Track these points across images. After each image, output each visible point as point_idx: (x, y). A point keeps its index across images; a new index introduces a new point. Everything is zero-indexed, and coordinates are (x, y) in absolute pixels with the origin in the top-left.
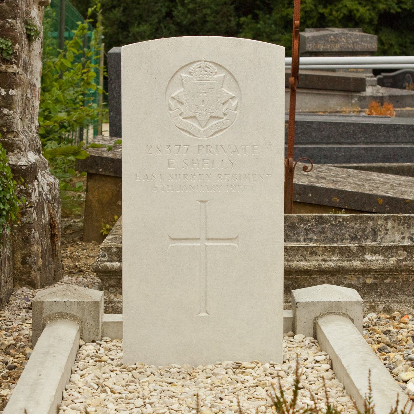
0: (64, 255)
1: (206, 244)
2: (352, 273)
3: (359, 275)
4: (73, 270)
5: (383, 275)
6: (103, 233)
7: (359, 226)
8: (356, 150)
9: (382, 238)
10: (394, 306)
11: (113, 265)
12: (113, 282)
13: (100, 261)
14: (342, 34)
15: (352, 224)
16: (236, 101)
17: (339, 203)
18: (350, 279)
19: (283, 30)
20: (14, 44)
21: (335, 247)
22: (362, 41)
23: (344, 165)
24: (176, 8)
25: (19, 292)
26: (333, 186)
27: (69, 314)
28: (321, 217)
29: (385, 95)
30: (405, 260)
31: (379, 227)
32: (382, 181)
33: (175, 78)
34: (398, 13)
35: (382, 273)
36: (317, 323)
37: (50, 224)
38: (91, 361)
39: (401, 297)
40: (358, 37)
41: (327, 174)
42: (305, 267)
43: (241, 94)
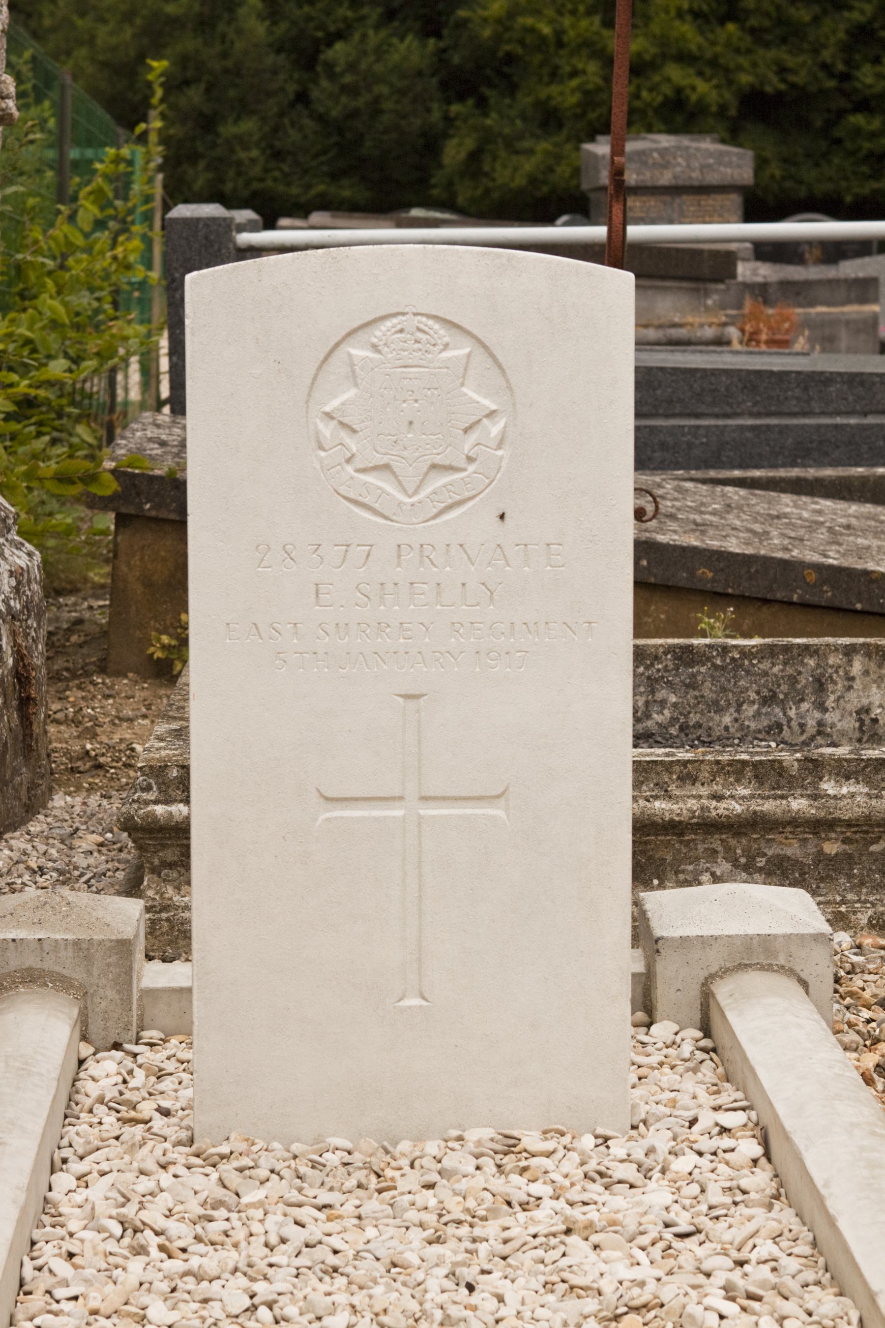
0: (59, 716)
1: (422, 812)
2: (788, 829)
3: (805, 832)
4: (79, 763)
5: (866, 832)
6: (153, 654)
7: (782, 671)
8: (733, 431)
9: (839, 698)
11: (171, 813)
12: (170, 855)
13: (137, 801)
14: (678, 148)
15: (765, 665)
16: (502, 424)
17: (713, 580)
18: (781, 843)
19: (539, 132)
21: (744, 763)
23: (712, 474)
26: (696, 539)
27: (51, 973)
28: (689, 649)
29: (769, 280)
31: (830, 671)
32: (806, 520)
33: (333, 360)
34: (779, 94)
36: (713, 995)
37: (17, 672)
38: (110, 1120)
40: (711, 154)
41: (677, 504)
42: (667, 814)
43: (514, 405)
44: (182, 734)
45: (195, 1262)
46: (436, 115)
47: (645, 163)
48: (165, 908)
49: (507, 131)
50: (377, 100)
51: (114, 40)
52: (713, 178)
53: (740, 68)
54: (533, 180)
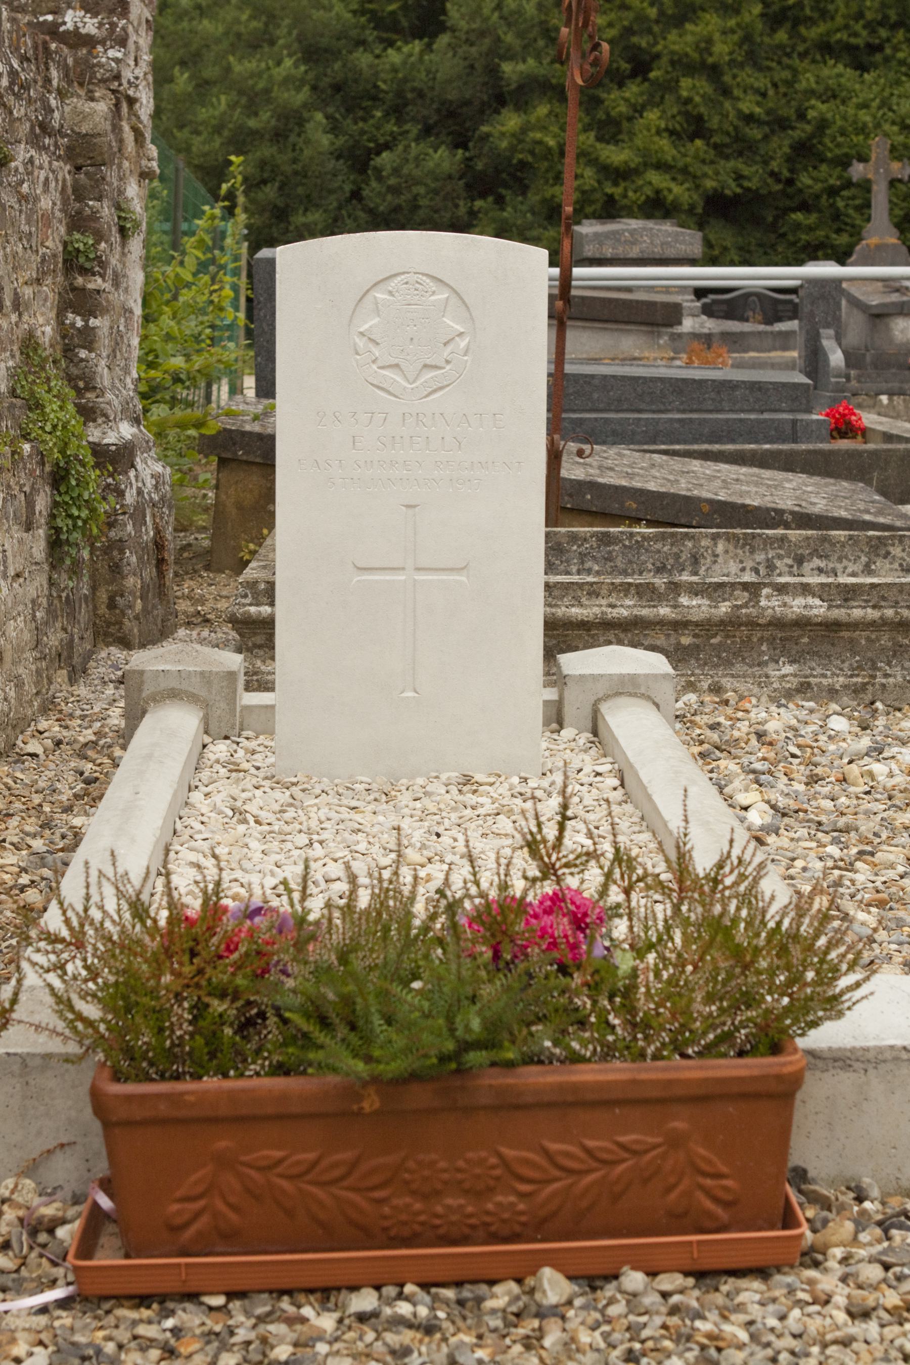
10: (726, 682)
12: (259, 639)
14: (644, 229)
15: (658, 546)
17: (637, 510)
20: (98, 242)
21: (630, 584)
22: (677, 241)
23: (646, 447)
25: (103, 654)
27: (186, 692)
28: (607, 534)
30: (745, 605)
33: (365, 300)
34: (736, 195)
35: (706, 627)
38: (223, 771)
39: (739, 668)
40: (669, 235)
47: (619, 240)
48: (255, 673)
49: (519, 222)
50: (415, 198)
51: (207, 148)
53: (705, 175)
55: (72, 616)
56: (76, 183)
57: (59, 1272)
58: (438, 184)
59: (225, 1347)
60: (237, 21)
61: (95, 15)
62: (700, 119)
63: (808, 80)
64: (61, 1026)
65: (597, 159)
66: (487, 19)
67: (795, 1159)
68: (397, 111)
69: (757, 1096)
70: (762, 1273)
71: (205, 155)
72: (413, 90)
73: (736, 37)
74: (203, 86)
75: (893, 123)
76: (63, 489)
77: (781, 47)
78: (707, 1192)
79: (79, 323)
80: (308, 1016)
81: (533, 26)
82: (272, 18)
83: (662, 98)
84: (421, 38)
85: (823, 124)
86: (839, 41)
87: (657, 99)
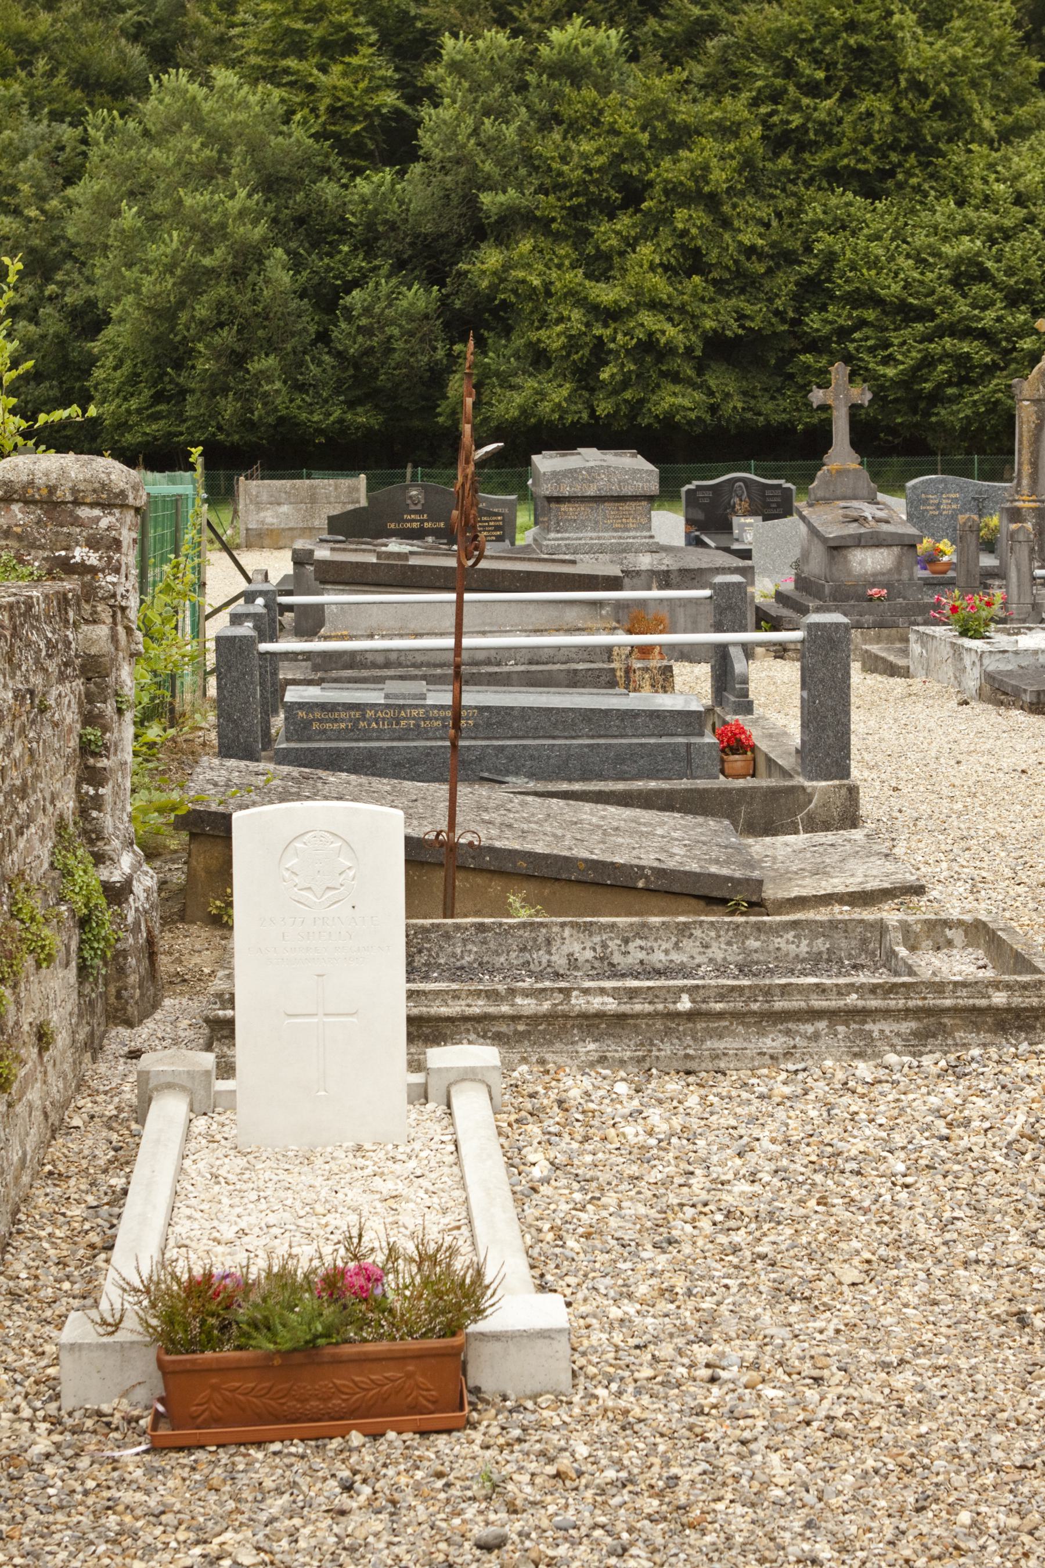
10: (549, 1057)
12: (225, 1033)
15: (521, 932)
20: (104, 733)
22: (634, 479)
24: (336, 326)
25: (113, 1033)
28: (482, 924)
30: (561, 1003)
35: (534, 1019)
38: (204, 1141)
39: (558, 1046)
44: (230, 977)
45: (238, 1187)
46: (440, 354)
47: (576, 479)
52: (628, 491)
53: (704, 315)
54: (523, 410)
55: (93, 1013)
56: (87, 690)
57: (142, 1439)
58: (414, 325)
59: (216, 1466)
60: (188, 150)
61: (97, 551)
62: (697, 252)
63: (814, 211)
64: (141, 1330)
65: (586, 298)
66: (464, 146)
67: (471, 1383)
68: (368, 246)
69: (443, 1355)
70: (449, 1431)
71: (156, 296)
72: (385, 222)
73: (734, 163)
74: (153, 221)
75: (908, 256)
76: (87, 929)
77: (785, 172)
78: (424, 1397)
79: (92, 792)
80: (249, 1325)
81: (514, 153)
82: (226, 149)
83: (656, 230)
84: (392, 165)
85: (830, 259)
86: (847, 166)
87: (650, 231)
